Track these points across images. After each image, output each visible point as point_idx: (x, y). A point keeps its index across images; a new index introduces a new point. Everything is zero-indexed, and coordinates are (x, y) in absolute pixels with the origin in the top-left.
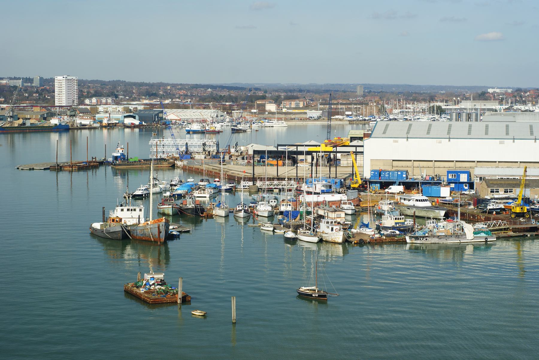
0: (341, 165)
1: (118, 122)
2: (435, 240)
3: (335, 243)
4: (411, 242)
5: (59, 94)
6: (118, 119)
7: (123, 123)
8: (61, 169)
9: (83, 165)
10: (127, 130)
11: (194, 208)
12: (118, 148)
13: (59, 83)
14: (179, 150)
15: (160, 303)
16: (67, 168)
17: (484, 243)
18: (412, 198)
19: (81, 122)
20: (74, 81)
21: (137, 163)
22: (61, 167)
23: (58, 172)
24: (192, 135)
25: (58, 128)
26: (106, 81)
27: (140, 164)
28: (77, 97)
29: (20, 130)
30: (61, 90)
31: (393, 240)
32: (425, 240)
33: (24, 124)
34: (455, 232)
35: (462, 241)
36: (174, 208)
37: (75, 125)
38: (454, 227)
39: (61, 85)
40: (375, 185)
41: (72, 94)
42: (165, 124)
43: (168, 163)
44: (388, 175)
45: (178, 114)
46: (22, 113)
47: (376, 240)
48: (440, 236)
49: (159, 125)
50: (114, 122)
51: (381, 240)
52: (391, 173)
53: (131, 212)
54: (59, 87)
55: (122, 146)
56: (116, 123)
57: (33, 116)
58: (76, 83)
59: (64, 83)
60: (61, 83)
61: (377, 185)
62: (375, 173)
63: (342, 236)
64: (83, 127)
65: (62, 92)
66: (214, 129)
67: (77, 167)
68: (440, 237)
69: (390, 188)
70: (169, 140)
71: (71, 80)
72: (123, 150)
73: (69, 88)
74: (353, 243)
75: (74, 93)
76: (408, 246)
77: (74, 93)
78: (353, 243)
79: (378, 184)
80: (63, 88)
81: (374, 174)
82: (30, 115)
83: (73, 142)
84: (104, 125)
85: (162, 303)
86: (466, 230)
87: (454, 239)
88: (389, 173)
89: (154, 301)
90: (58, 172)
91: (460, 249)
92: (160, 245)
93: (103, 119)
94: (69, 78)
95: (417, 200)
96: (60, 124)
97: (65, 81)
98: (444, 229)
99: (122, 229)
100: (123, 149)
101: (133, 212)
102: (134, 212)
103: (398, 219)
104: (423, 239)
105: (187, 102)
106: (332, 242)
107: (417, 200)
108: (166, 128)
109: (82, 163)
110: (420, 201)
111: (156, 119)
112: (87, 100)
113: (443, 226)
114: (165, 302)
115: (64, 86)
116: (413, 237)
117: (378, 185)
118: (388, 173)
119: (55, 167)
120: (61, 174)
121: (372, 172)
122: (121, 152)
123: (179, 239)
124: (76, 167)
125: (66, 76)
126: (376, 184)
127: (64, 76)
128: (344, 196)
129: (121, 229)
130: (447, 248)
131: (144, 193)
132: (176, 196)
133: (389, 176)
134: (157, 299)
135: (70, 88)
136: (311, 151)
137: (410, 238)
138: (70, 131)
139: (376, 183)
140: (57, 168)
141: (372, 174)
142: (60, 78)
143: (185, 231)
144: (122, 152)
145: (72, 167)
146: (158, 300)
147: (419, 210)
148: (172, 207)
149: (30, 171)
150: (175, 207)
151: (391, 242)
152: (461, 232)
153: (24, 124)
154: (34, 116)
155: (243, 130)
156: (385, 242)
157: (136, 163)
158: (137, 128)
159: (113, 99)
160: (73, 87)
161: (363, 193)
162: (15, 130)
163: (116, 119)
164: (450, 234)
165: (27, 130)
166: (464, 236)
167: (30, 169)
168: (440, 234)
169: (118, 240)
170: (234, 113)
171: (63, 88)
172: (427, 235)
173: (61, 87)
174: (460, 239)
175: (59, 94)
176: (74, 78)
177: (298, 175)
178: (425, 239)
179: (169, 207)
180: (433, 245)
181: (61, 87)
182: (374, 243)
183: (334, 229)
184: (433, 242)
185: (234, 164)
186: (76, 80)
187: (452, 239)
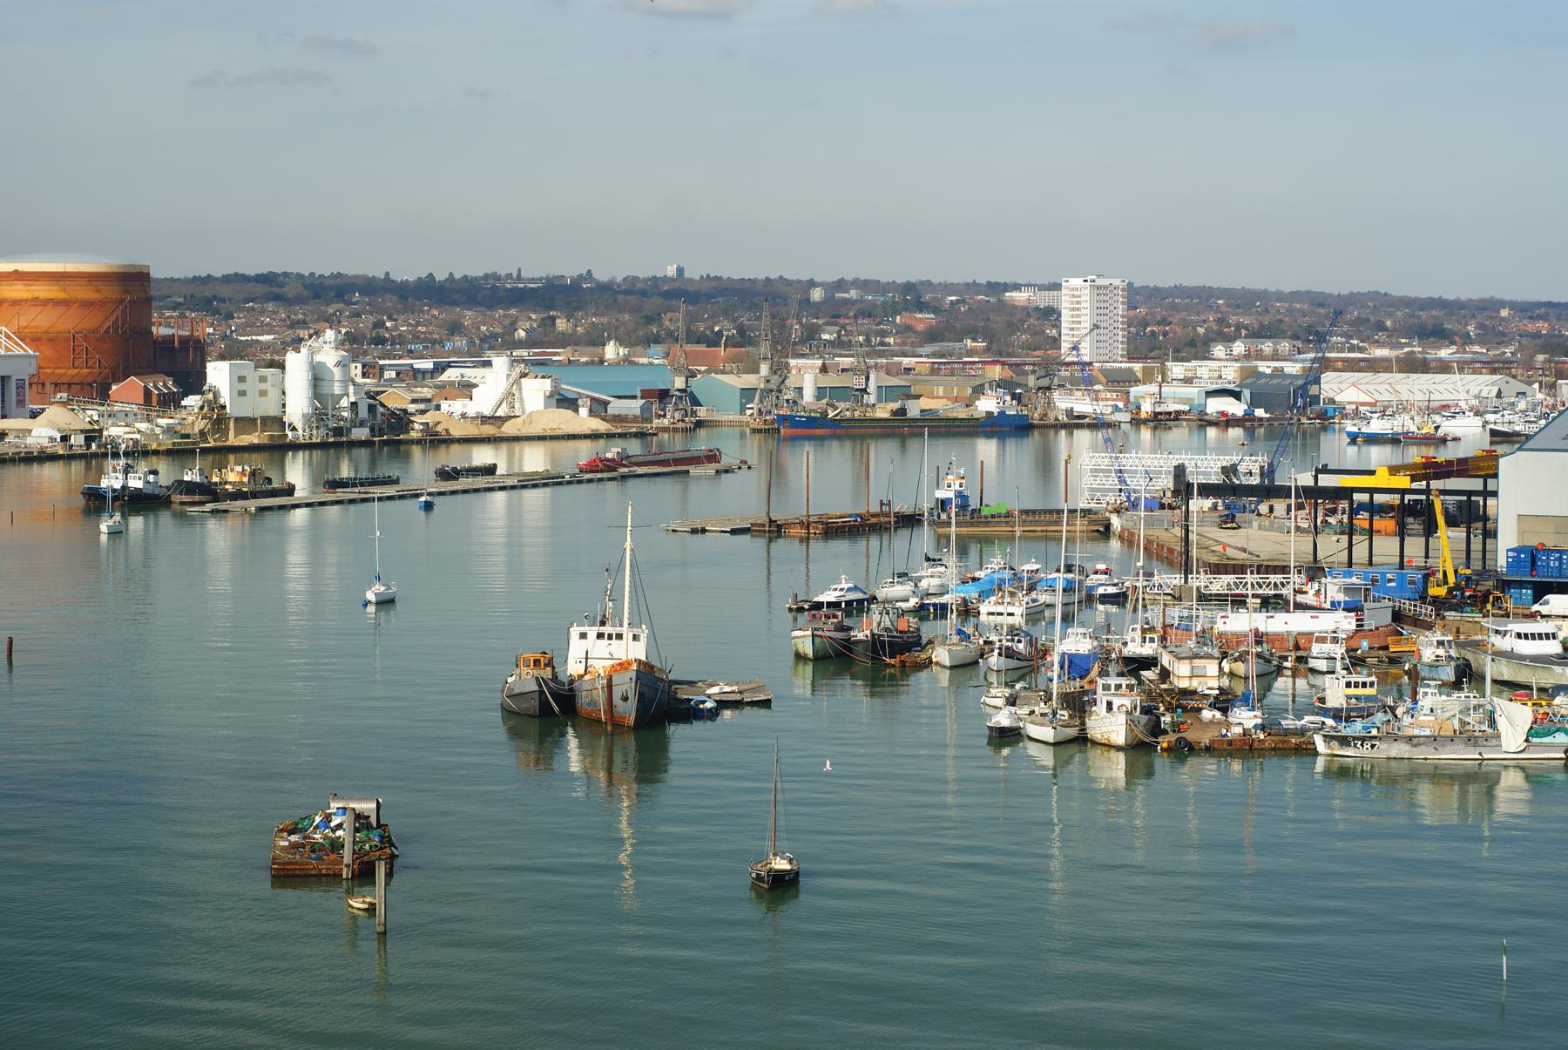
0: (979, 507)
1: (1187, 408)
2: (1399, 750)
3: (1109, 746)
4: (1329, 752)
5: (1072, 329)
6: (1188, 399)
7: (1203, 412)
8: (779, 531)
9: (843, 522)
10: (1212, 432)
11: (869, 641)
12: (949, 477)
13: (1073, 296)
14: (1127, 485)
15: (298, 876)
16: (794, 528)
17: (1563, 762)
18: (1509, 627)
19: (1072, 408)
20: (1115, 292)
21: (999, 520)
22: (779, 526)
23: (770, 541)
24: (1364, 448)
25: (992, 425)
26: (1474, 298)
27: (1007, 522)
28: (1124, 336)
29: (883, 427)
30: (1079, 316)
31: (1285, 746)
32: (1369, 746)
33: (902, 411)
34: (1467, 728)
35: (1486, 756)
36: (818, 640)
37: (1051, 416)
38: (1466, 711)
39: (1078, 303)
40: (1518, 591)
41: (1111, 328)
42: (1323, 415)
43: (1089, 522)
44: (1557, 564)
45: (1371, 388)
46: (927, 381)
47: (1230, 743)
48: (1415, 737)
49: (1304, 420)
50: (1173, 407)
51: (1245, 744)
52: (1565, 557)
53: (610, 642)
54: (1073, 309)
55: (962, 472)
56: (1178, 413)
57: (953, 389)
58: (1123, 296)
59: (1086, 296)
60: (1079, 297)
61: (1524, 591)
62: (1518, 557)
63: (1125, 727)
64: (1075, 422)
65: (1079, 322)
66: (1432, 431)
67: (821, 526)
68: (1415, 741)
69: (1547, 603)
70: (1208, 457)
71: (1106, 287)
72: (963, 481)
73: (1101, 311)
74: (1159, 748)
75: (1115, 325)
76: (1320, 764)
77: (1115, 325)
78: (1159, 748)
79: (1528, 589)
80: (1084, 311)
81: (1516, 559)
82: (945, 386)
83: (1045, 464)
84: (1143, 415)
85: (305, 876)
86: (1502, 723)
87: (1462, 747)
88: (1561, 557)
89: (283, 870)
90: (770, 541)
91: (1482, 780)
92: (612, 732)
93: (1141, 401)
94: (1100, 282)
95: (1519, 636)
96: (1002, 413)
97: (1087, 291)
98: (1433, 718)
99: (540, 686)
100: (963, 478)
101: (614, 642)
102: (618, 641)
103: (1355, 687)
104: (1362, 745)
105: (1505, 353)
106: (1104, 745)
107: (1519, 636)
108: (1324, 429)
109: (842, 518)
110: (1526, 636)
111: (1300, 402)
112: (1218, 348)
113: (1432, 710)
114: (314, 872)
115: (1087, 305)
116: (1332, 738)
117: (1529, 591)
118: (1557, 555)
119: (764, 525)
120: (780, 545)
121: (1510, 554)
122: (957, 488)
123: (1327, 465)
124: (817, 528)
125: (1095, 277)
126: (1521, 588)
127: (1089, 278)
128: (1349, 620)
129: (536, 688)
130: (1438, 775)
131: (842, 599)
132: (932, 610)
133: (1561, 563)
134: (291, 863)
135: (1105, 311)
136: (1348, 488)
137: (1325, 741)
138: (1036, 433)
139: (1521, 584)
140: (767, 529)
141: (1510, 560)
142: (1077, 282)
143: (752, 701)
144: (961, 486)
145: (808, 528)
146: (293, 867)
147: (1516, 665)
148: (813, 636)
149: (694, 536)
150: (821, 637)
151: (1280, 749)
152: (1485, 727)
153: (902, 411)
154: (955, 388)
155: (1524, 435)
156: (1262, 749)
157: (996, 519)
158: (1238, 426)
159: (1294, 346)
160: (1111, 308)
161: (1453, 613)
162: (869, 427)
163: (1182, 401)
164: (1450, 733)
165: (903, 427)
166: (1494, 742)
167: (694, 531)
168: (1416, 732)
169: (529, 715)
170: (1561, 385)
171: (1084, 311)
172: (1374, 732)
173: (1079, 309)
174: (1480, 749)
175: (1072, 329)
176: (1117, 282)
177: (1320, 555)
178: (1368, 745)
179: (805, 636)
180: (1393, 763)
181: (1079, 309)
182: (1225, 750)
183: (1115, 707)
184: (1393, 754)
185: (1260, 528)
186: (1123, 290)
187: (1455, 747)
